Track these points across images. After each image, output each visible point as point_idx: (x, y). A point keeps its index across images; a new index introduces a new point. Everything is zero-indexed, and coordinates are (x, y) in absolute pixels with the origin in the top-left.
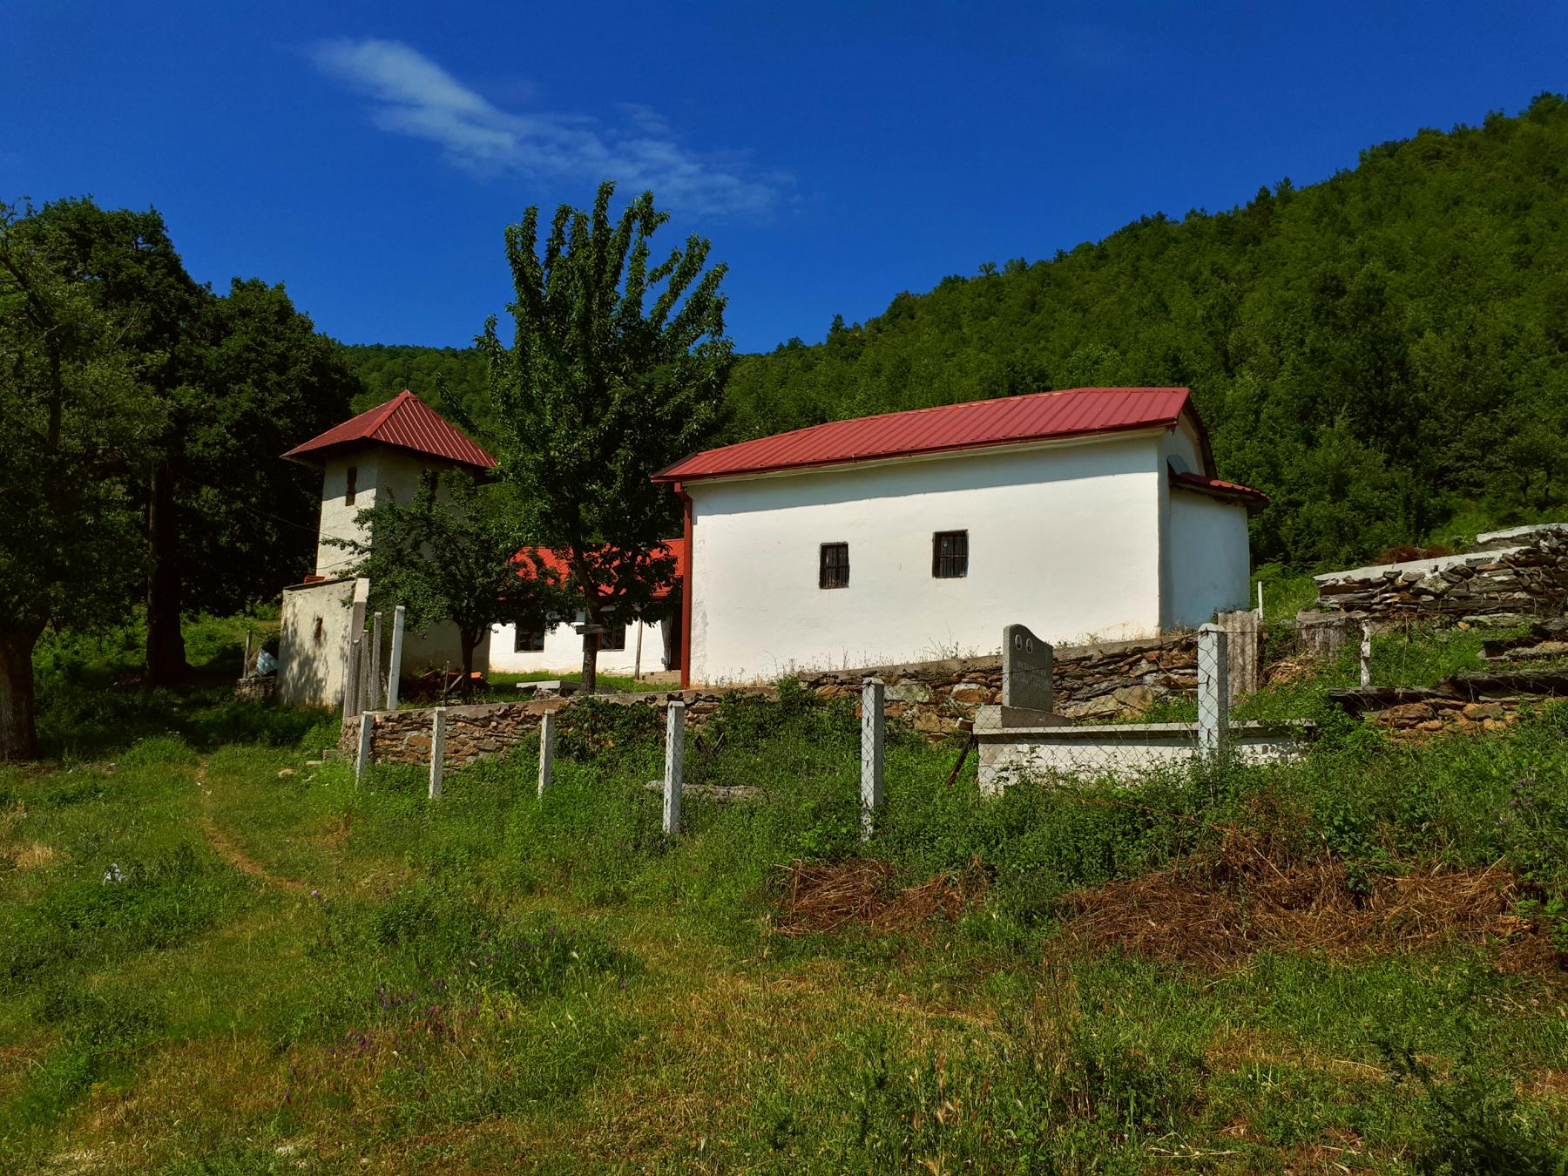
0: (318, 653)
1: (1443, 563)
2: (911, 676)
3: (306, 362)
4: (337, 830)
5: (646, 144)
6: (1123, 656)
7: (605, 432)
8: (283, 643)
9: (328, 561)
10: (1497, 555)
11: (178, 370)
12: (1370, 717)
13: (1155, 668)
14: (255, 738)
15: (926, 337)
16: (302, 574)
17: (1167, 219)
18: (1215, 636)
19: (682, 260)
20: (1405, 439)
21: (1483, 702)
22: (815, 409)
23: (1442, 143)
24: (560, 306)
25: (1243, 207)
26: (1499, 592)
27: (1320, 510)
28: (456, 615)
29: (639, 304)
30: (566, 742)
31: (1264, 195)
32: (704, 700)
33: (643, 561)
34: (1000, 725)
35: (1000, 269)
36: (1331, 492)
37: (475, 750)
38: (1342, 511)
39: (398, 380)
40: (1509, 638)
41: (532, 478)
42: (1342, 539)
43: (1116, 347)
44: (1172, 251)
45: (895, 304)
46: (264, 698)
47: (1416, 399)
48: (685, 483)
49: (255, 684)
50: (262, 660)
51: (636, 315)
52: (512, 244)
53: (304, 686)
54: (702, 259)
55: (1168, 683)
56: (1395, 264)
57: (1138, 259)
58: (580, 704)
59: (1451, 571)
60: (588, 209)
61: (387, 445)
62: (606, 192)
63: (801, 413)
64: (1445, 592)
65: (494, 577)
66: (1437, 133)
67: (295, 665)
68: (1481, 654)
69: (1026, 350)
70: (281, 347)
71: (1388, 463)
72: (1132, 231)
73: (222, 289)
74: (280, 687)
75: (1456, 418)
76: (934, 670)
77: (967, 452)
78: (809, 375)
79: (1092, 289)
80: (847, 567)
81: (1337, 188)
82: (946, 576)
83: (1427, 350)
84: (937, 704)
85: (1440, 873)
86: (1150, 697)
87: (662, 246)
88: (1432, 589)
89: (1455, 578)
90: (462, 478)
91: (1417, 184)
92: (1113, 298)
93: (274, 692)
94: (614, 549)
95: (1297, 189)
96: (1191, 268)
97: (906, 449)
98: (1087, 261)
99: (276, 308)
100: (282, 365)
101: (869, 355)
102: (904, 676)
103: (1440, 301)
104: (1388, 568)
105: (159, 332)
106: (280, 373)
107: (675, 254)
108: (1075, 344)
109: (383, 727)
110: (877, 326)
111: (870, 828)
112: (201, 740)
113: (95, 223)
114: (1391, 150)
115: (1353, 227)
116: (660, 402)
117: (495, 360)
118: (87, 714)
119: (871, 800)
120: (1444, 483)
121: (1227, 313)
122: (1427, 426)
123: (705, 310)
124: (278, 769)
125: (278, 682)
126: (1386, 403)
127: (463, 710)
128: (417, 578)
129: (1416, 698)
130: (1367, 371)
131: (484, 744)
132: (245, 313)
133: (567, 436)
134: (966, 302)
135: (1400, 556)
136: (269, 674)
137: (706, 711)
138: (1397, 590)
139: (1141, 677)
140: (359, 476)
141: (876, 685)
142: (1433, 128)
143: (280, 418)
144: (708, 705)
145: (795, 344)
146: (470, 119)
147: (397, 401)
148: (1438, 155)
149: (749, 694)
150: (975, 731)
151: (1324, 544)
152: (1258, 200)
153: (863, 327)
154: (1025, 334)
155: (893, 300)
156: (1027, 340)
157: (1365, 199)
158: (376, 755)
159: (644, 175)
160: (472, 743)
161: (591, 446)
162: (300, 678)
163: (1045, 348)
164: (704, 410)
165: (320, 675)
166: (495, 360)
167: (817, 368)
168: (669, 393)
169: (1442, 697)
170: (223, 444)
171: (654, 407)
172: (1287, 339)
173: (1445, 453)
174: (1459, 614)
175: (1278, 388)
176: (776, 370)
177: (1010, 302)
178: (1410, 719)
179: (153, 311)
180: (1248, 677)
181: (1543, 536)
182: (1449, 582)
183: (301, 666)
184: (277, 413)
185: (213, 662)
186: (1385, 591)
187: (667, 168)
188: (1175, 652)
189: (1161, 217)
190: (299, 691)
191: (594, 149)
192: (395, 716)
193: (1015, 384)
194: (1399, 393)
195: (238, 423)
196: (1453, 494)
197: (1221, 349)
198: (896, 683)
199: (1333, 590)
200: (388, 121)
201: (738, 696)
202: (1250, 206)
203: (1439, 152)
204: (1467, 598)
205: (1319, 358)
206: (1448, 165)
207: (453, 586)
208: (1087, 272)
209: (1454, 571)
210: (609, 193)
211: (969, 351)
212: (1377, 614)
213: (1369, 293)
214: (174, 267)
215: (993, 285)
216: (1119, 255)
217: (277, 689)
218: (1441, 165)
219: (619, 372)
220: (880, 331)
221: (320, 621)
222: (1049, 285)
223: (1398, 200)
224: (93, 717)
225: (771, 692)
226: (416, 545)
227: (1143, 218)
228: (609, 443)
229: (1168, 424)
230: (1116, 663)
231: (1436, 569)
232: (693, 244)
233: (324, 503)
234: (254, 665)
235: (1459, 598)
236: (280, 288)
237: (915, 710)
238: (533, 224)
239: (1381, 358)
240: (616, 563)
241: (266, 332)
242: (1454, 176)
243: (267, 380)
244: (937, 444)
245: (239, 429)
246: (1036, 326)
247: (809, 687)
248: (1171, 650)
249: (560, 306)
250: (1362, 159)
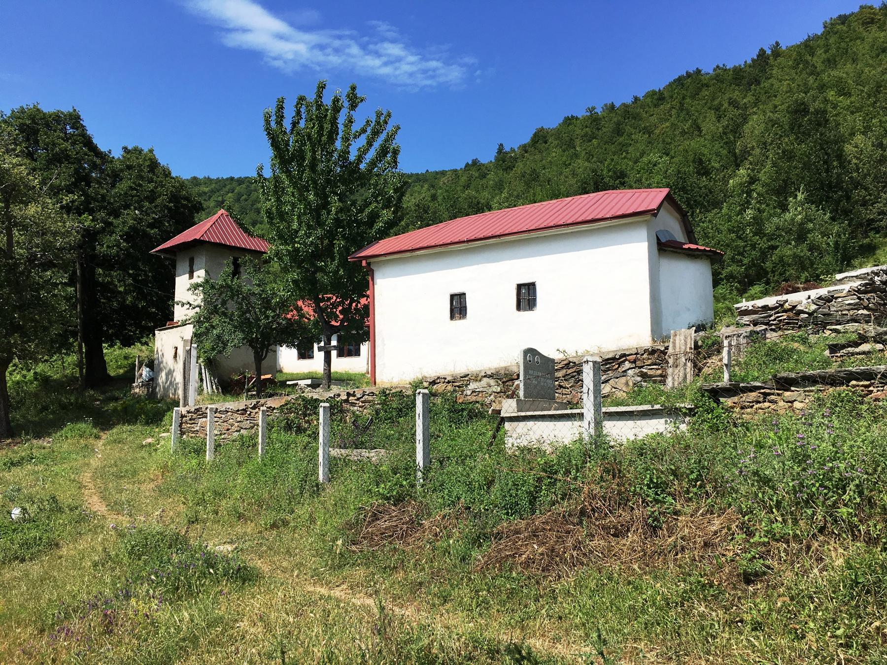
0: (175, 368)
1: (814, 293)
2: (491, 376)
3: (166, 195)
4: (157, 479)
5: (386, 45)
6: (614, 359)
7: (327, 230)
8: (156, 362)
9: (180, 313)
10: (846, 287)
11: (91, 204)
12: (728, 402)
13: (634, 365)
14: (137, 420)
15: (554, 154)
16: (165, 319)
17: (703, 72)
18: (591, 364)
19: (372, 125)
20: (844, 203)
21: (793, 391)
22: (478, 203)
23: (874, 14)
24: (299, 156)
25: (749, 62)
26: (849, 310)
27: (787, 251)
28: (251, 343)
29: (349, 152)
30: (289, 422)
31: (762, 53)
32: (368, 395)
33: (357, 305)
34: (516, 410)
35: (599, 110)
36: (795, 240)
37: (238, 429)
38: (803, 250)
39: (243, 197)
40: (842, 341)
41: (286, 259)
42: (803, 268)
43: (667, 155)
44: (705, 93)
45: (535, 135)
47: (851, 178)
48: (372, 260)
50: (145, 372)
51: (347, 159)
52: (268, 122)
53: (169, 387)
54: (386, 122)
55: (644, 376)
56: (844, 92)
57: (684, 98)
58: (297, 399)
59: (818, 298)
60: (311, 97)
61: (209, 242)
62: (322, 87)
63: (469, 207)
64: (815, 311)
65: (271, 319)
66: (871, 8)
67: (163, 374)
68: (827, 353)
69: (612, 160)
70: (151, 186)
71: (833, 219)
72: (680, 81)
73: (117, 154)
75: (877, 188)
76: (502, 372)
77: (534, 235)
78: (484, 181)
79: (654, 119)
80: (466, 307)
81: (809, 46)
82: (525, 310)
83: (856, 147)
84: (505, 392)
85: (702, 515)
86: (631, 384)
87: (362, 116)
88: (807, 310)
89: (821, 303)
90: (251, 261)
91: (858, 41)
92: (667, 124)
94: (338, 300)
95: (784, 48)
96: (716, 103)
97: (496, 234)
98: (652, 102)
99: (148, 163)
100: (152, 198)
101: (520, 167)
102: (485, 376)
103: (868, 115)
104: (779, 298)
105: (81, 180)
106: (150, 203)
107: (368, 121)
108: (642, 154)
109: (186, 417)
110: (525, 148)
111: (421, 481)
112: (104, 422)
113: (41, 119)
114: (843, 19)
115: (818, 69)
116: (361, 211)
117: (264, 190)
118: (45, 408)
119: (421, 464)
120: (871, 229)
121: (736, 129)
122: (858, 194)
123: (389, 152)
124: (145, 438)
125: (154, 385)
126: (830, 182)
127: (231, 405)
128: (225, 322)
129: (755, 389)
130: (818, 162)
131: (243, 425)
132: (129, 167)
133: (305, 234)
134: (578, 131)
135: (787, 290)
136: (150, 380)
137: (369, 402)
138: (785, 311)
139: (625, 371)
140: (195, 262)
141: (423, 394)
142: (869, 5)
143: (152, 229)
144: (370, 398)
145: (475, 162)
146: (280, 37)
147: (216, 217)
148: (872, 21)
149: (394, 391)
150: (503, 414)
151: (792, 272)
152: (758, 56)
153: (516, 150)
154: (613, 150)
155: (534, 133)
156: (614, 154)
157: (826, 52)
158: (182, 433)
159: (386, 64)
160: (236, 424)
161: (321, 239)
162: (166, 382)
163: (625, 158)
164: (387, 215)
166: (264, 190)
167: (488, 177)
168: (367, 204)
169: (769, 389)
170: (118, 246)
171: (357, 213)
172: (771, 144)
173: (871, 210)
174: (824, 326)
175: (763, 177)
176: (463, 179)
177: (604, 130)
178: (750, 402)
179: (75, 169)
180: (688, 370)
181: (877, 274)
182: (817, 305)
183: (167, 375)
184: (152, 226)
185: (126, 372)
186: (778, 313)
187: (399, 59)
188: (645, 356)
189: (698, 71)
190: (166, 390)
191: (355, 50)
192: (193, 410)
193: (597, 185)
194: (839, 175)
195: (127, 234)
196: (878, 236)
197: (732, 152)
198: (480, 381)
199: (746, 312)
200: (234, 40)
201: (388, 392)
202: (753, 60)
203: (873, 19)
204: (829, 315)
205: (788, 155)
206: (879, 28)
207: (245, 325)
208: (652, 109)
209: (820, 298)
210: (323, 87)
211: (579, 161)
212: (773, 327)
213: (818, 114)
214: (88, 142)
215: (594, 120)
216: (672, 97)
217: (154, 389)
218: (874, 28)
219: (336, 194)
220: (526, 152)
222: (629, 118)
223: (847, 51)
224: (47, 410)
225: (407, 389)
226: (224, 303)
227: (687, 72)
228: (331, 235)
229: (654, 213)
230: (610, 363)
231: (809, 298)
232: (379, 114)
233: (177, 279)
234: (141, 375)
235: (824, 315)
236: (151, 151)
237: (492, 397)
238: (282, 108)
239: (826, 154)
240: (341, 308)
241: (142, 178)
242: (882, 35)
243: (143, 207)
244: (515, 231)
245: (129, 236)
246: (620, 144)
247: (429, 385)
248: (642, 355)
249: (299, 156)
250: (825, 27)
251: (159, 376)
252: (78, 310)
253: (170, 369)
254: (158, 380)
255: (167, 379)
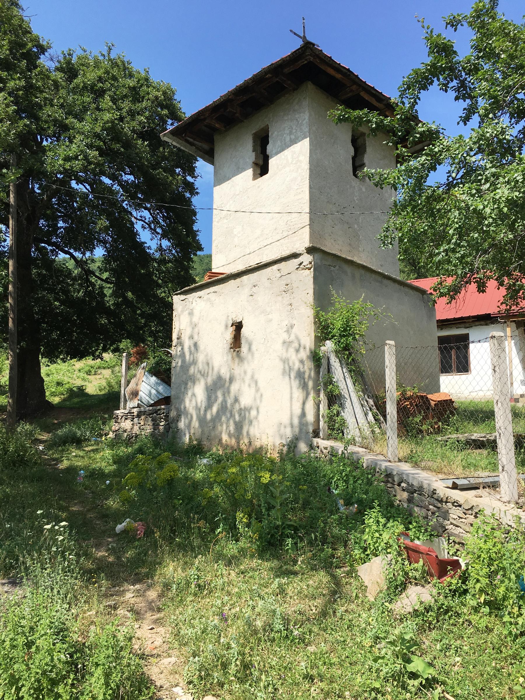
46: (152, 435)
49: (139, 416)
74: (177, 419)
93: (168, 427)
125: (173, 414)
136: (158, 403)
162: (209, 406)
165: (245, 401)
185: (64, 400)
221: (238, 326)
234: (135, 394)
251: (185, 393)
252: (11, 268)
253: (220, 378)
254: (183, 400)
255: (210, 402)
